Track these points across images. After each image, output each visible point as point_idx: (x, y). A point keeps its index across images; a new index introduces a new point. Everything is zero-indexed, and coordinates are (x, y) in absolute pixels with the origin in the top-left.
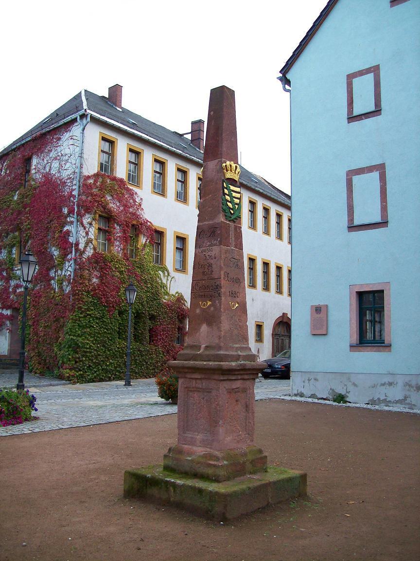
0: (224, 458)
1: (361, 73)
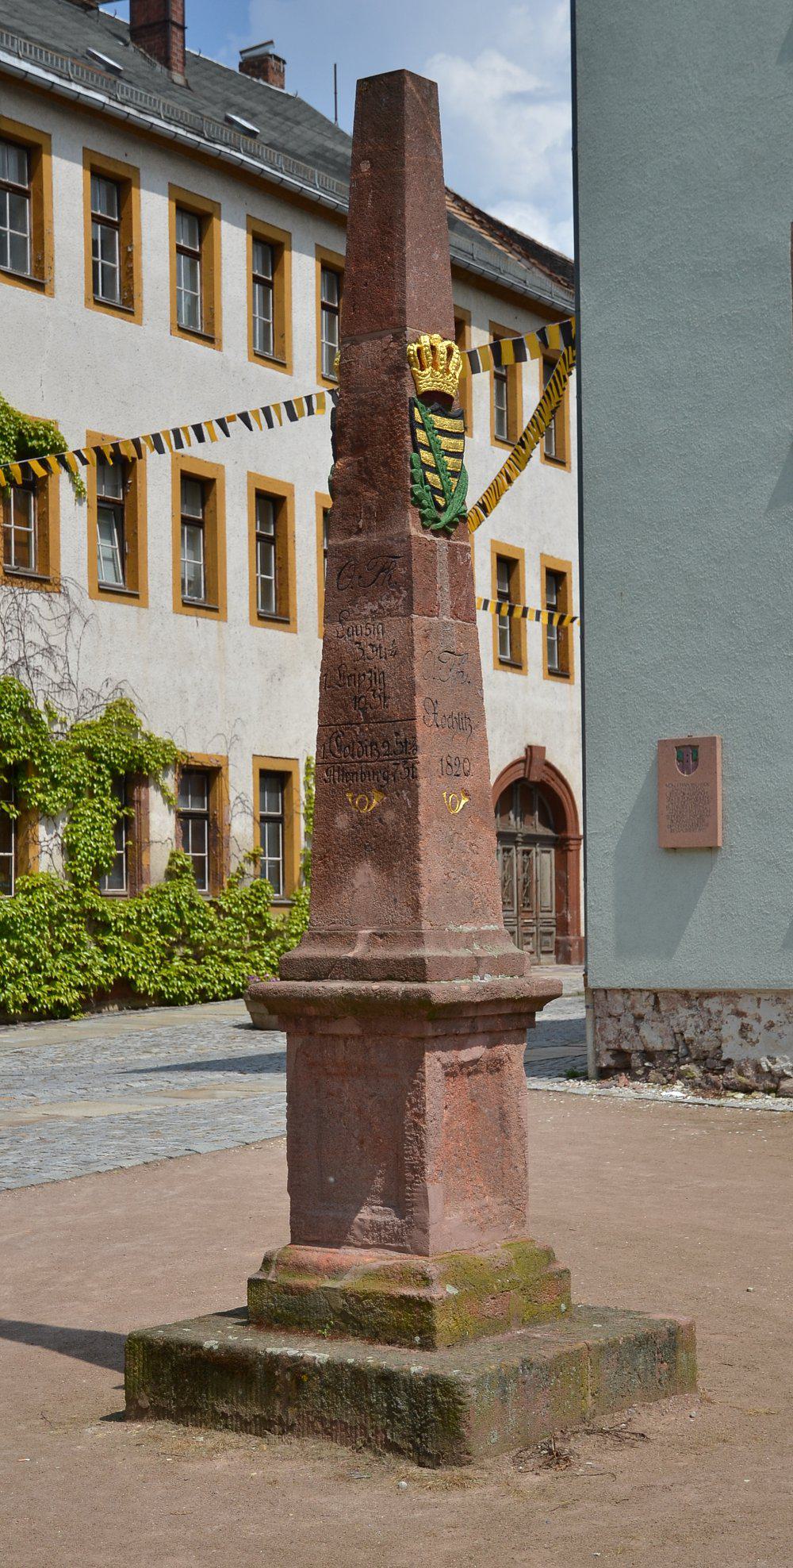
0: (445, 1278)
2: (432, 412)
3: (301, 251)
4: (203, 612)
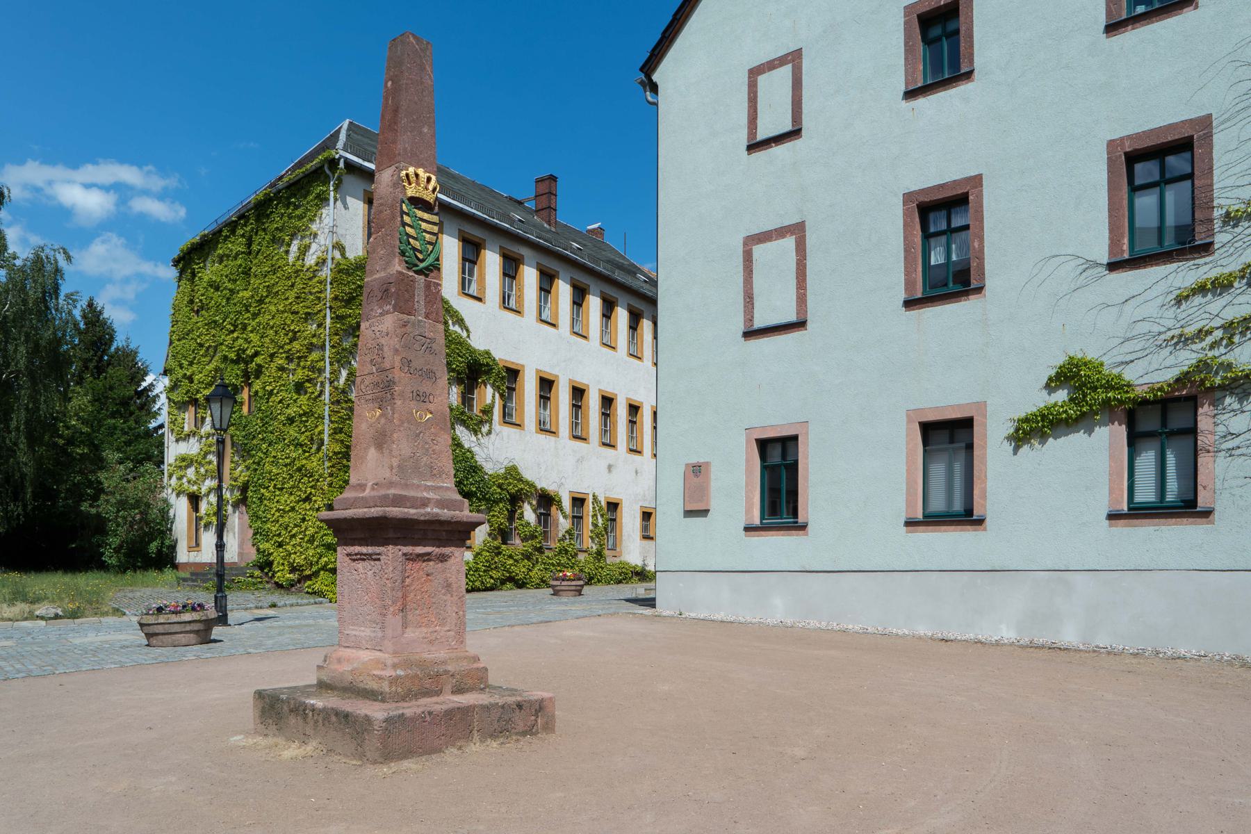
1: (771, 66)
3: (593, 295)
4: (548, 433)
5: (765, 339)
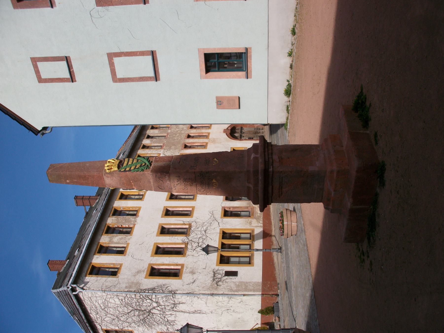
1: (37, 72)
2: (122, 166)
5: (160, 70)
